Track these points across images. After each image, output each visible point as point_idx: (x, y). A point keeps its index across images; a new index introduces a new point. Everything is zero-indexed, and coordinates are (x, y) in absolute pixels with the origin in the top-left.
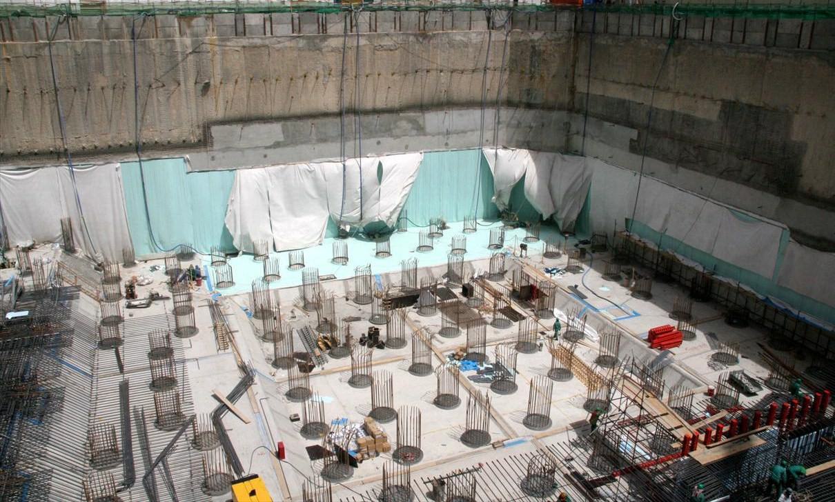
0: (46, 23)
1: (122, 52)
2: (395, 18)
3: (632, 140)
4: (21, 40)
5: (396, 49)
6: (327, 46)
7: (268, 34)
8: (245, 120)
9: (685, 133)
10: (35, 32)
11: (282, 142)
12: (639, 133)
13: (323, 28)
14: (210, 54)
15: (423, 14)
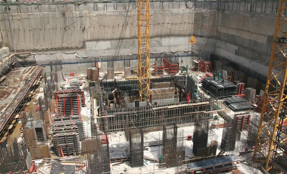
3: (236, 50)
4: (23, 13)
5: (151, 16)
8: (97, 40)
9: (254, 48)
14: (85, 17)
15: (161, 3)
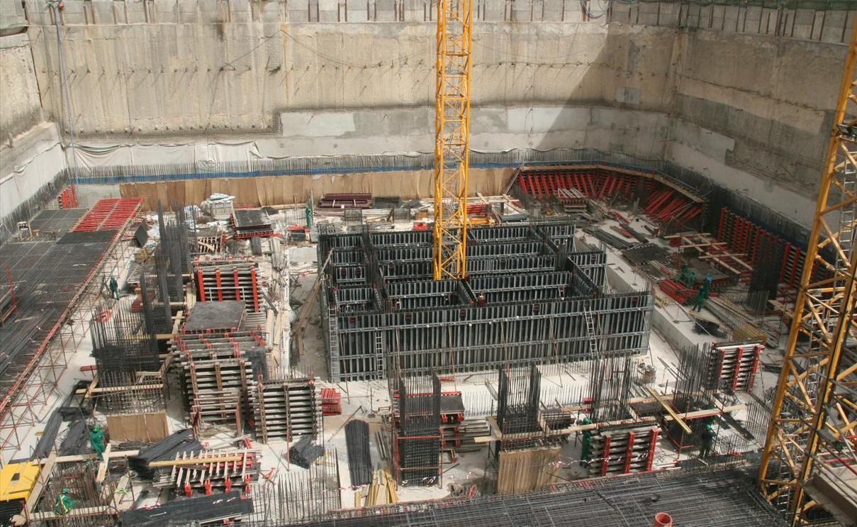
0: (125, 7)
1: (195, 36)
2: (479, 6)
6: (404, 35)
7: (342, 20)
10: (114, 15)
11: (353, 132)
12: (736, 145)
13: (400, 15)
